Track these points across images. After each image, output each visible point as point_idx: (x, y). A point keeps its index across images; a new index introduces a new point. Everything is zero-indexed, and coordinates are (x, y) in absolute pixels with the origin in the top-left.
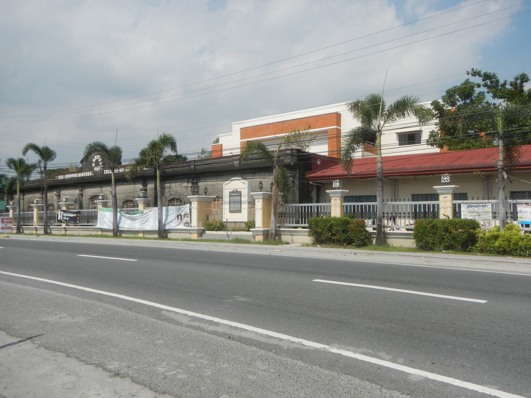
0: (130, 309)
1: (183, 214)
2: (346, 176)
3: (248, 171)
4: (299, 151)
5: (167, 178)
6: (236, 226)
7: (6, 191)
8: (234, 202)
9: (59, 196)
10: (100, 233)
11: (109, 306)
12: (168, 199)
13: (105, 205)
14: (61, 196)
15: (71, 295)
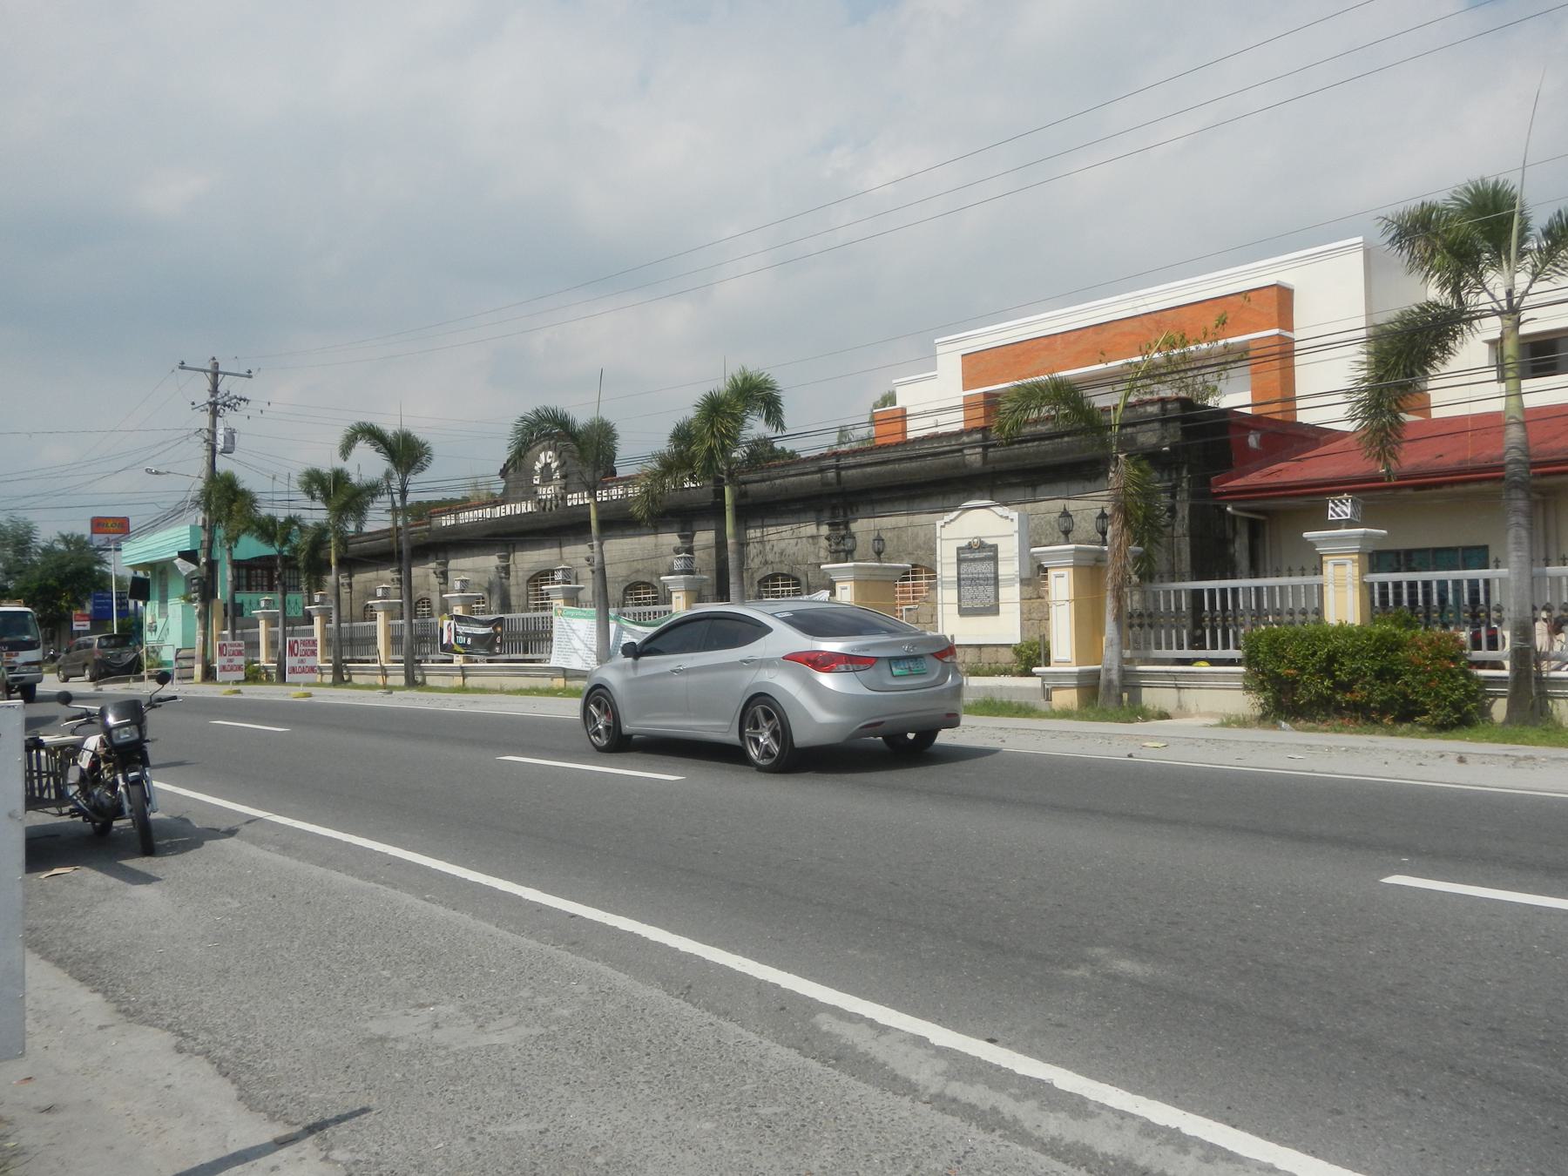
0: (687, 993)
2: (1381, 479)
3: (1014, 480)
4: (1186, 404)
5: (757, 510)
6: (987, 660)
7: (301, 565)
8: (974, 581)
9: (444, 575)
10: (559, 682)
11: (610, 972)
12: (758, 577)
13: (573, 599)
15: (474, 916)
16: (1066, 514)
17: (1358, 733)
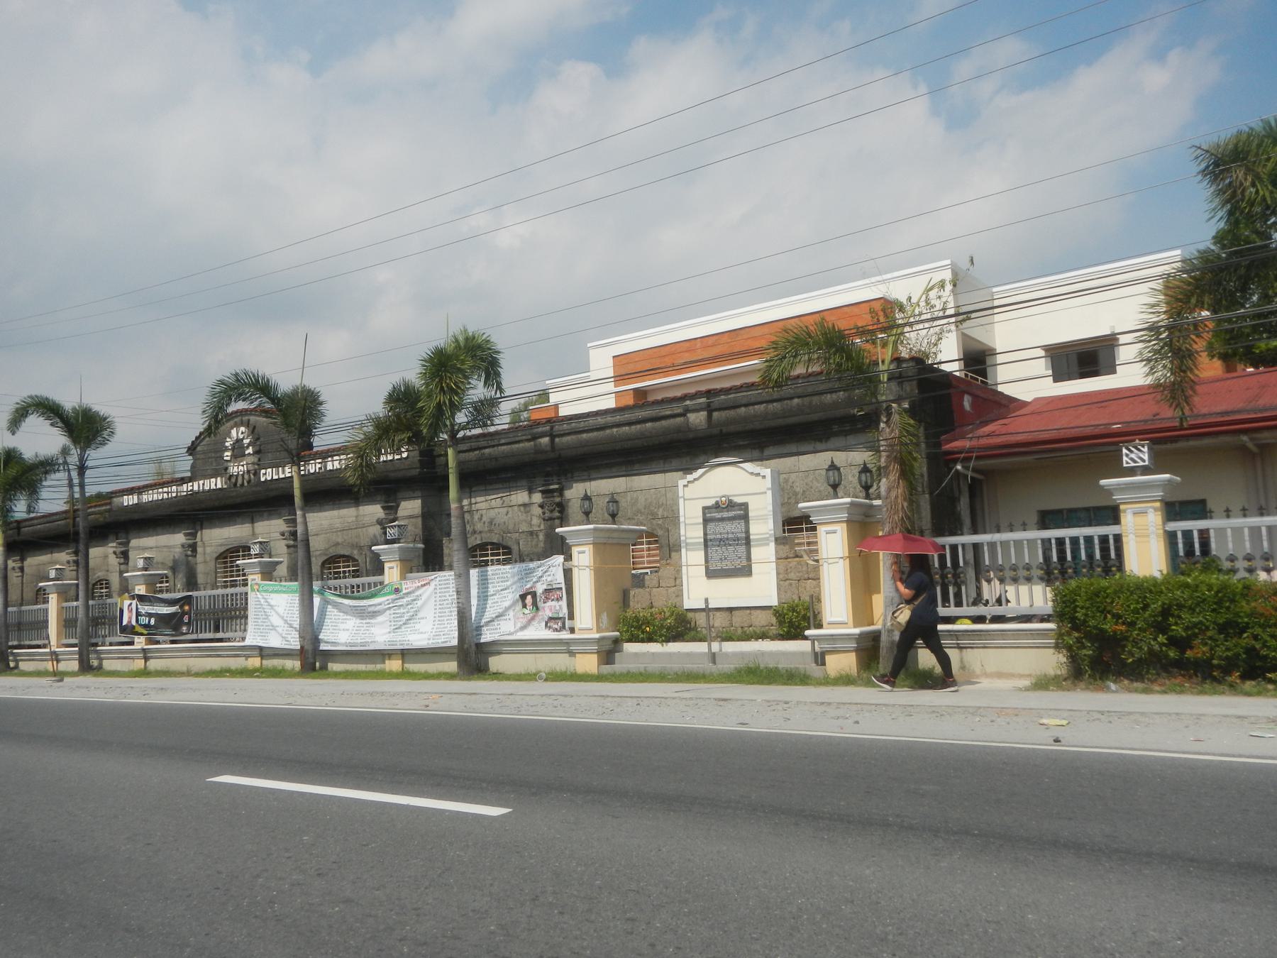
1: (540, 589)
6: (736, 624)
8: (723, 542)
9: (125, 555)
10: (255, 662)
13: (268, 573)
14: (131, 554)
16: (833, 467)
17: (1202, 693)
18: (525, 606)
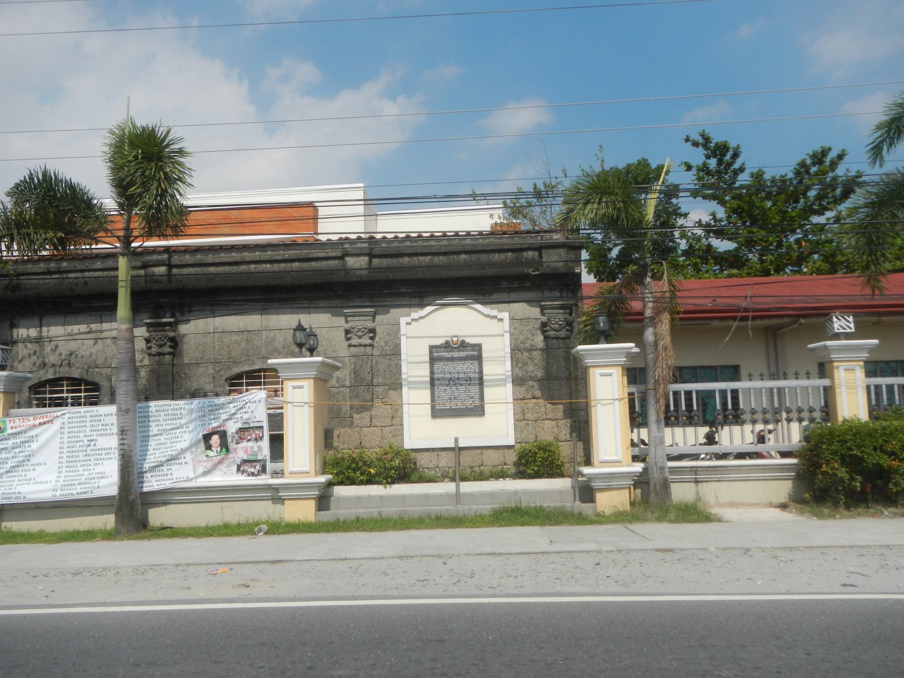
6: (464, 464)
8: (452, 382)
18: (209, 447)
